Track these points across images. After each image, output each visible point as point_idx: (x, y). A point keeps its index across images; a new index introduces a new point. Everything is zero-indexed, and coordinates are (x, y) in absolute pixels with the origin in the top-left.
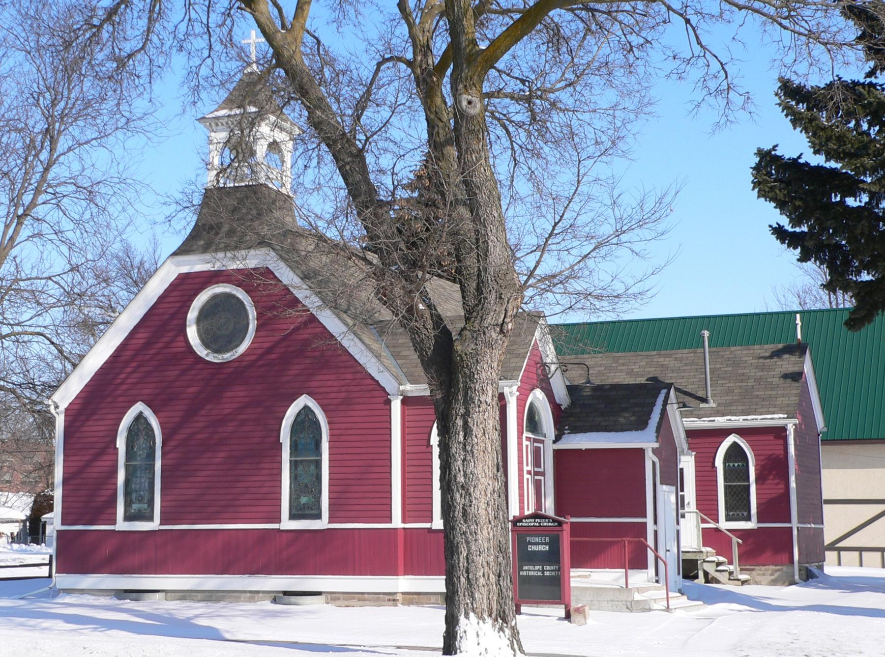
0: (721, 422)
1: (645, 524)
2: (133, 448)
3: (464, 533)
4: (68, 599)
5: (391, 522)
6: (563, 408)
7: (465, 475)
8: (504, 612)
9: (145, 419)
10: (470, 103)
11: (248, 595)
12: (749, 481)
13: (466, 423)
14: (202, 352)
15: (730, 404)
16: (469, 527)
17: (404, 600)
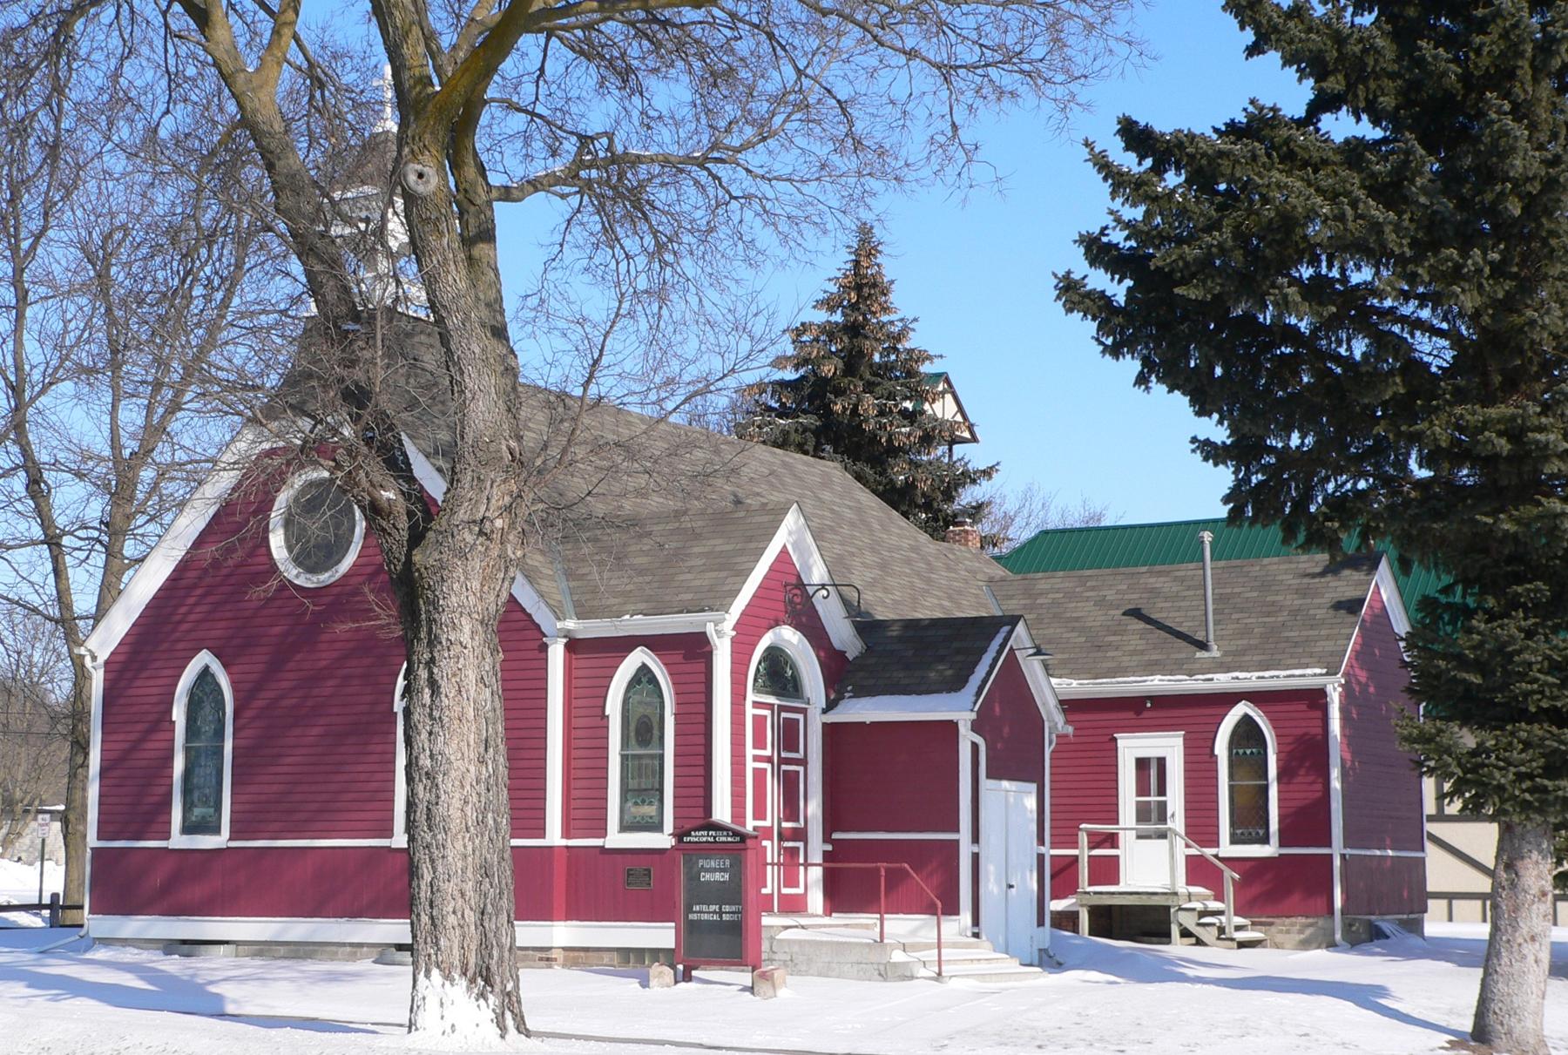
0: (1223, 681)
2: (195, 721)
3: (428, 847)
4: (101, 954)
5: (543, 836)
6: (850, 656)
7: (432, 756)
8: (488, 969)
9: (213, 676)
10: (421, 176)
11: (348, 949)
12: (1266, 778)
13: (431, 673)
14: (292, 572)
15: (1243, 652)
16: (434, 836)
17: (566, 959)
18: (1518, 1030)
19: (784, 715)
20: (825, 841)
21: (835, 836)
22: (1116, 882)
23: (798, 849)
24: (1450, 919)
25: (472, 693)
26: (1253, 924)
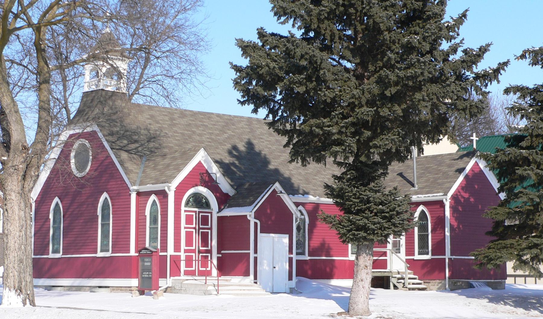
1: (249, 253)
5: (129, 253)
18: (356, 308)
19: (201, 214)
20: (218, 253)
21: (222, 252)
22: (386, 268)
23: (208, 256)
24: (536, 283)
25: (17, 213)
26: (424, 282)
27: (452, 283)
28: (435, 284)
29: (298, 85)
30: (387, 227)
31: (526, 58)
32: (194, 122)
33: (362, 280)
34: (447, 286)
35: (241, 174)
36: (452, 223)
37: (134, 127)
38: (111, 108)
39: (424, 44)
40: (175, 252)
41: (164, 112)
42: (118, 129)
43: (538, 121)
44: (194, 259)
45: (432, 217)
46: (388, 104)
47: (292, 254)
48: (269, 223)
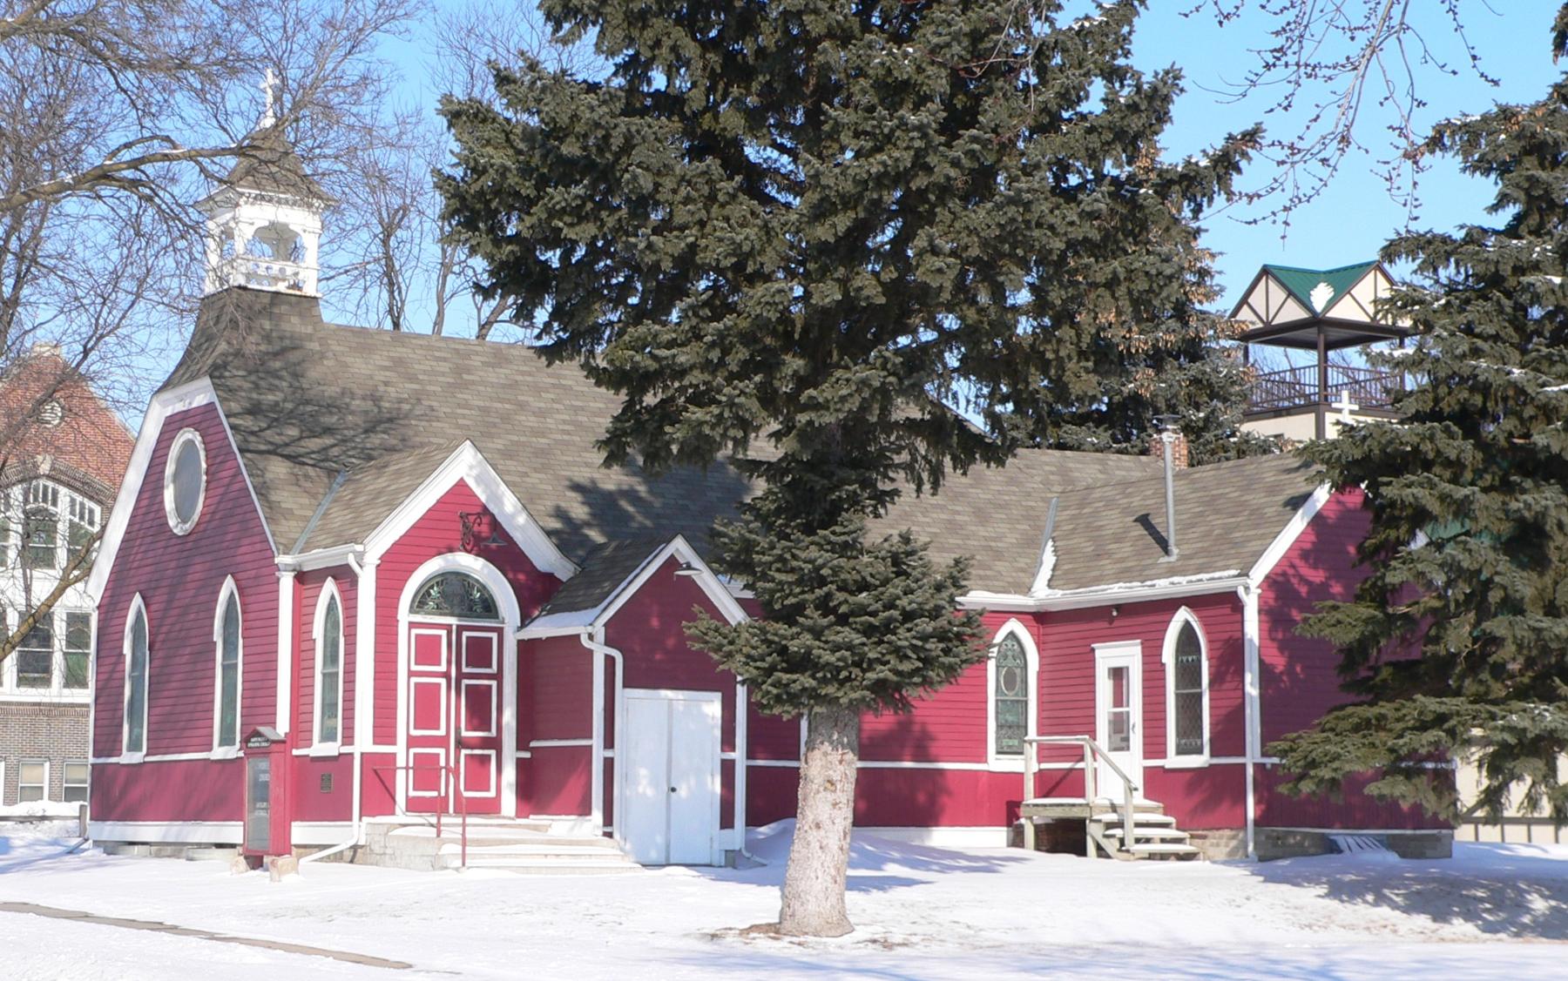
0: (1163, 587)
19: (465, 634)
20: (519, 748)
21: (533, 744)
26: (1192, 837)
27: (1268, 837)
28: (1220, 842)
29: (568, 219)
30: (877, 659)
31: (1444, 148)
32: (529, 379)
33: (818, 826)
34: (1251, 848)
35: (648, 523)
36: (1268, 660)
37: (331, 391)
38: (267, 338)
39: (931, 70)
40: (375, 743)
41: (439, 349)
42: (279, 396)
43: (1453, 334)
44: (443, 763)
45: (1210, 641)
46: (836, 269)
47: (733, 749)
48: (658, 657)
